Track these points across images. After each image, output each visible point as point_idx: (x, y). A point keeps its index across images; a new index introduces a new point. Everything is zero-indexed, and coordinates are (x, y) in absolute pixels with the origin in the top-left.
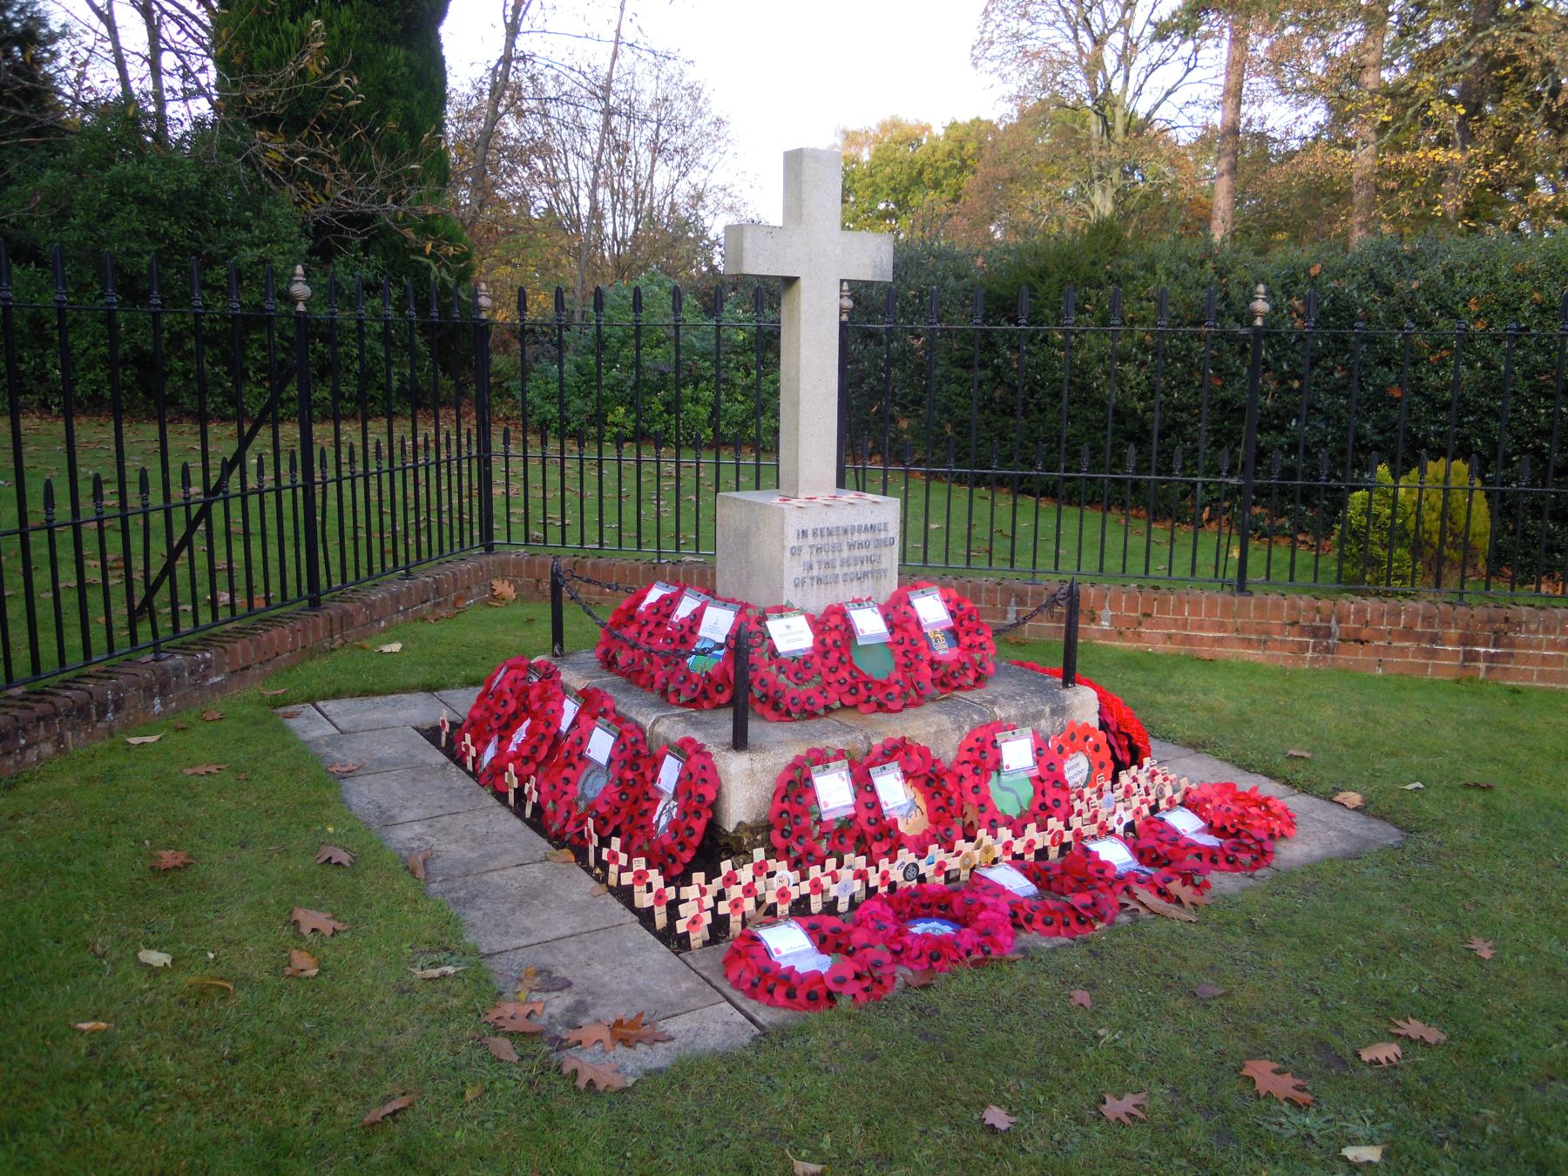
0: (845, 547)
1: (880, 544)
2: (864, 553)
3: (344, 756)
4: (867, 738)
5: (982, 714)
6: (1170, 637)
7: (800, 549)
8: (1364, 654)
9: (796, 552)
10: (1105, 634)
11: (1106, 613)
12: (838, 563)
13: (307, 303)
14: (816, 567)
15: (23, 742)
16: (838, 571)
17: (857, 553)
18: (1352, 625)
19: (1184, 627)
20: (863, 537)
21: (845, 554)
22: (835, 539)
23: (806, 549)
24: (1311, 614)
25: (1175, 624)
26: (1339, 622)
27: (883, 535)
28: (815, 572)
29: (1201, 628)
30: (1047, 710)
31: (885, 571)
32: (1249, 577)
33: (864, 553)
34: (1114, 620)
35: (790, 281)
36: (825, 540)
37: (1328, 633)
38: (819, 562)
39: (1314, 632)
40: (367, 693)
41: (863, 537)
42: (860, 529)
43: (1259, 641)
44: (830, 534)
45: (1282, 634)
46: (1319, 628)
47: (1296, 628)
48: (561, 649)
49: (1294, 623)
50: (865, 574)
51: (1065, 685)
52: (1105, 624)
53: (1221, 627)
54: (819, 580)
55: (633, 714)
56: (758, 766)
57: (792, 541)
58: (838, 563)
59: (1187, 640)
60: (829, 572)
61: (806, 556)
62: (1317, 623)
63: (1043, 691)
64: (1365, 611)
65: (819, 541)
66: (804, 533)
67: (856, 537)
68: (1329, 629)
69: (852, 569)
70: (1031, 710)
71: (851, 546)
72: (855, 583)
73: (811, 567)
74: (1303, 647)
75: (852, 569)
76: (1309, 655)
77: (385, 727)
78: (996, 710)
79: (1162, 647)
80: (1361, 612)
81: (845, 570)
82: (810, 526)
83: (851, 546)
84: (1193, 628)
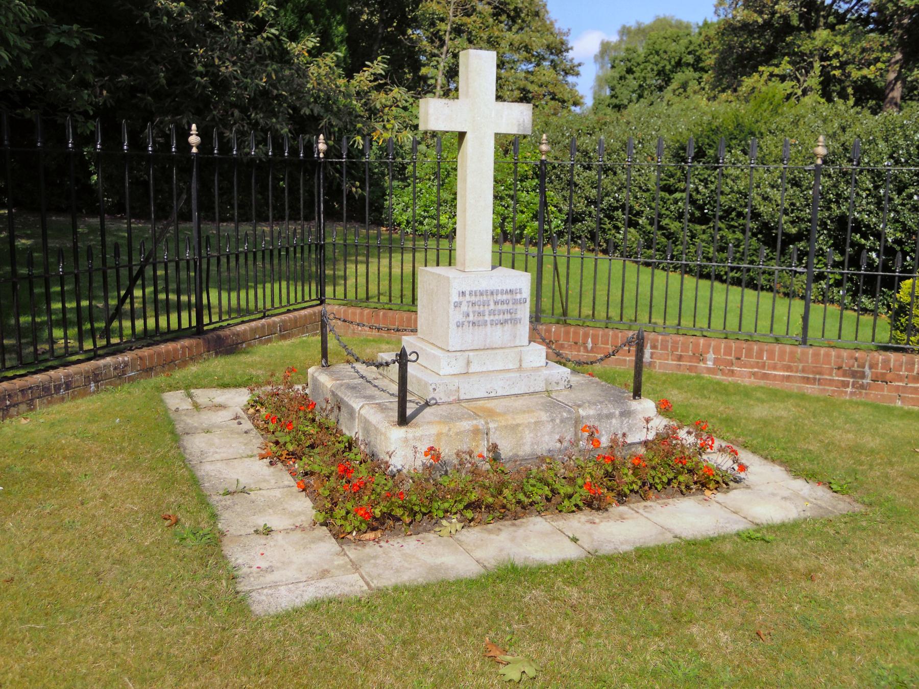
0: (492, 303)
1: (515, 302)
2: (505, 307)
3: (193, 421)
4: (487, 423)
5: (569, 412)
6: (754, 374)
7: (461, 303)
8: (889, 391)
9: (457, 305)
10: (709, 370)
11: (711, 356)
12: (487, 313)
13: (405, 73)
14: (471, 315)
15: (8, 403)
16: (487, 318)
17: (500, 307)
18: (880, 370)
19: (763, 367)
20: (505, 297)
21: (492, 307)
22: (485, 298)
23: (464, 304)
24: (851, 362)
25: (757, 365)
26: (871, 367)
27: (518, 296)
28: (471, 318)
29: (775, 368)
30: (617, 412)
31: (520, 320)
32: (810, 333)
33: (505, 307)
34: (716, 361)
35: (462, 135)
36: (478, 298)
37: (863, 376)
38: (474, 312)
39: (854, 374)
40: (225, 386)
41: (505, 297)
42: (503, 292)
43: (815, 379)
44: (481, 294)
45: (831, 375)
46: (857, 372)
47: (840, 372)
48: (326, 362)
49: (839, 368)
50: (506, 321)
51: (634, 398)
52: (710, 364)
53: (789, 368)
54: (474, 323)
55: (345, 399)
56: (410, 435)
57: (455, 298)
58: (487, 313)
59: (765, 376)
60: (481, 318)
61: (464, 308)
62: (855, 368)
63: (618, 400)
64: (889, 361)
65: (473, 299)
66: (463, 293)
67: (500, 297)
68: (864, 372)
69: (497, 317)
70: (605, 412)
71: (496, 303)
72: (499, 326)
73: (468, 315)
74: (845, 384)
75: (497, 317)
76: (849, 390)
77: (221, 407)
78: (581, 411)
79: (747, 382)
80: (886, 362)
81: (492, 317)
82: (467, 289)
83: (496, 303)
84: (769, 369)
